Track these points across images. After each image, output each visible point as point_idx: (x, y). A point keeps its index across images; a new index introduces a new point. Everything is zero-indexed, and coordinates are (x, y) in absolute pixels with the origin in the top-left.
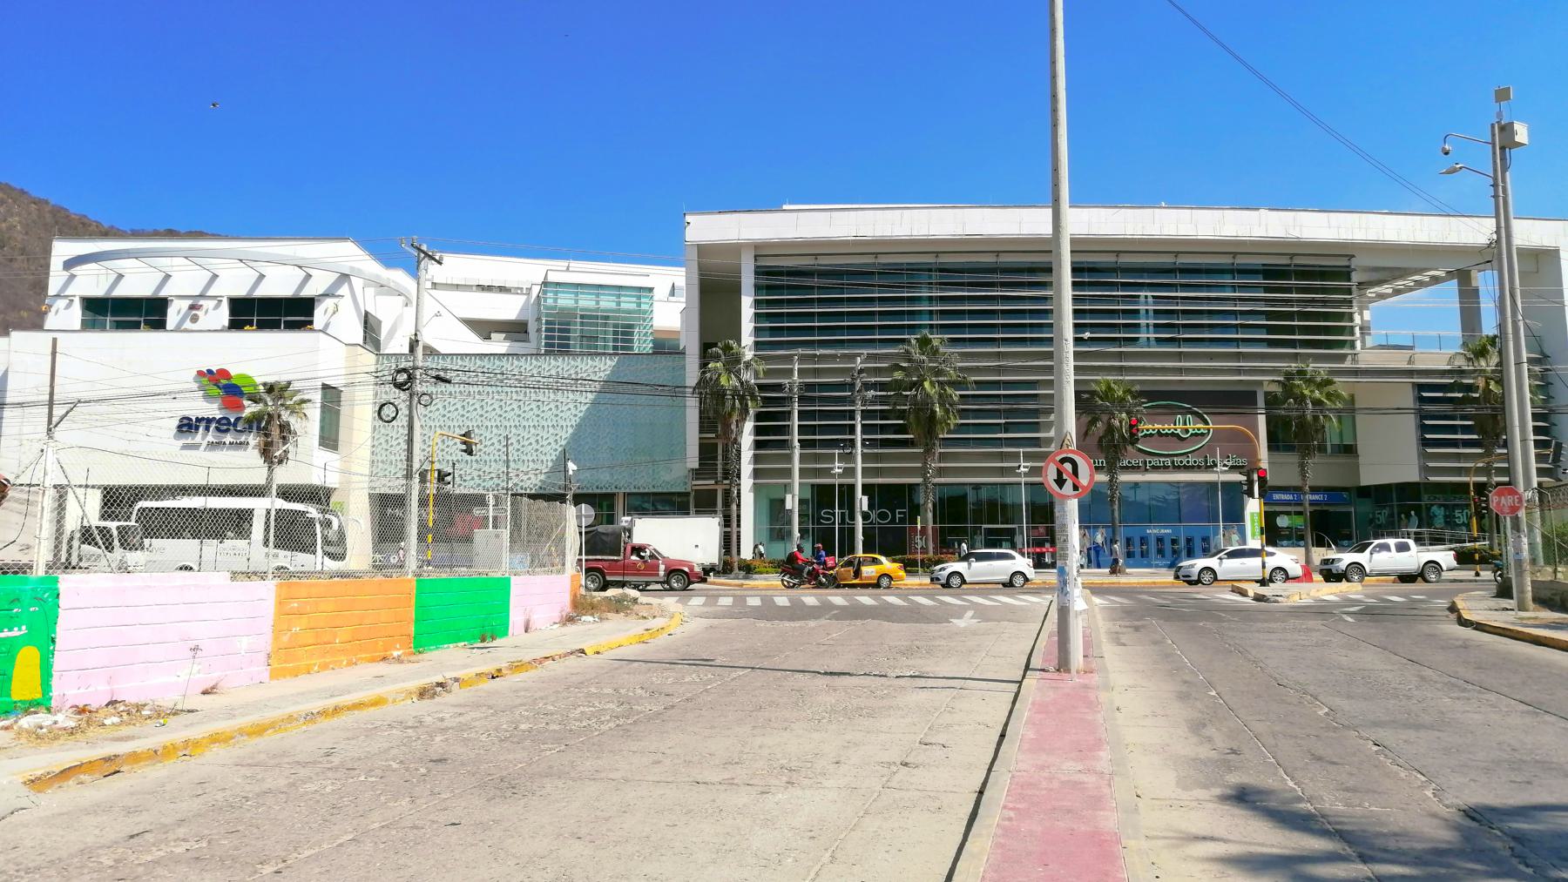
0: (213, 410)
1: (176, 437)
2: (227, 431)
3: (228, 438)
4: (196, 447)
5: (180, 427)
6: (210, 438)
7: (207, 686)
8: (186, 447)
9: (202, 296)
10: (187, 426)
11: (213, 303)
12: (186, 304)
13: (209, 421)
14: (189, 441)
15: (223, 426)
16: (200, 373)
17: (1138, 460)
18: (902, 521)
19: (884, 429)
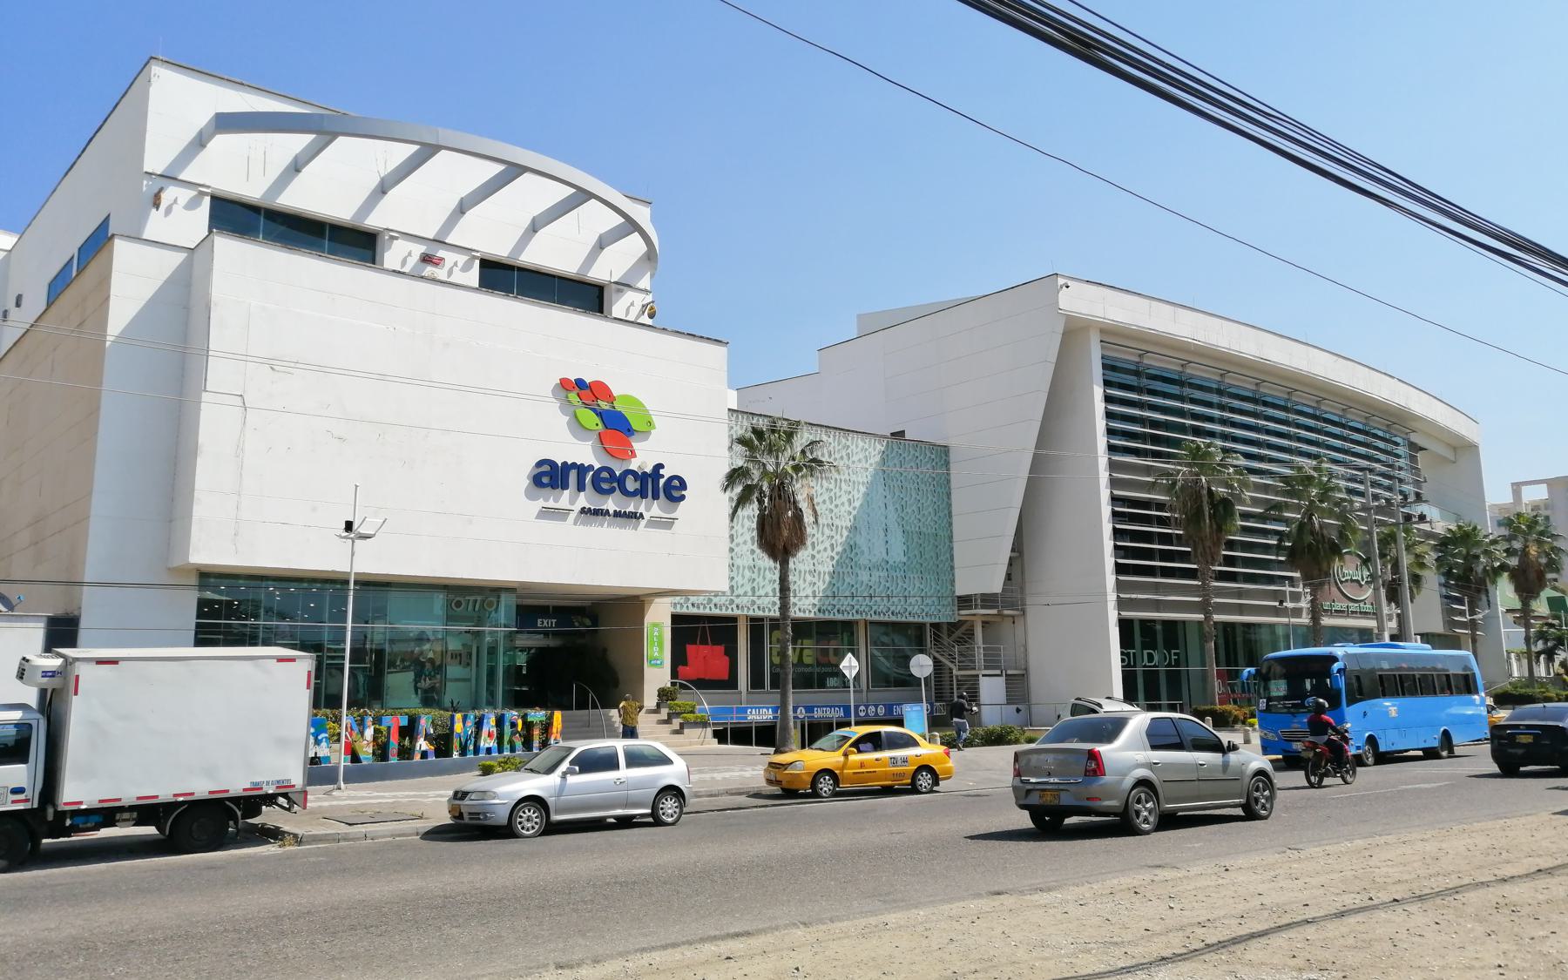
0: (585, 453)
1: (529, 495)
2: (612, 491)
3: (611, 504)
4: (558, 514)
5: (537, 481)
6: (583, 501)
7: (24, 302)
8: (546, 513)
9: (439, 242)
10: (550, 476)
11: (187, 194)
12: (419, 249)
13: (582, 470)
14: (551, 504)
15: (606, 481)
16: (565, 384)
17: (1340, 605)
18: (1178, 663)
19: (1136, 536)
